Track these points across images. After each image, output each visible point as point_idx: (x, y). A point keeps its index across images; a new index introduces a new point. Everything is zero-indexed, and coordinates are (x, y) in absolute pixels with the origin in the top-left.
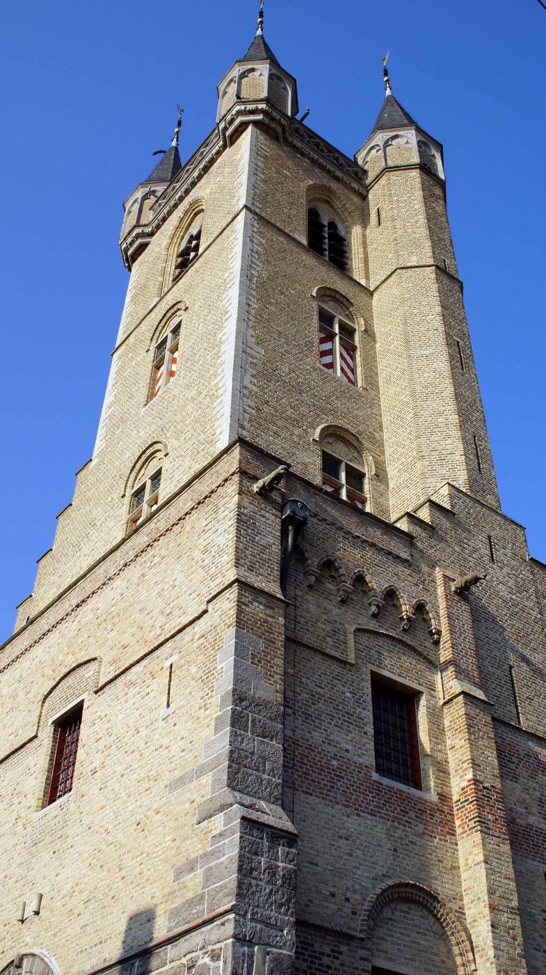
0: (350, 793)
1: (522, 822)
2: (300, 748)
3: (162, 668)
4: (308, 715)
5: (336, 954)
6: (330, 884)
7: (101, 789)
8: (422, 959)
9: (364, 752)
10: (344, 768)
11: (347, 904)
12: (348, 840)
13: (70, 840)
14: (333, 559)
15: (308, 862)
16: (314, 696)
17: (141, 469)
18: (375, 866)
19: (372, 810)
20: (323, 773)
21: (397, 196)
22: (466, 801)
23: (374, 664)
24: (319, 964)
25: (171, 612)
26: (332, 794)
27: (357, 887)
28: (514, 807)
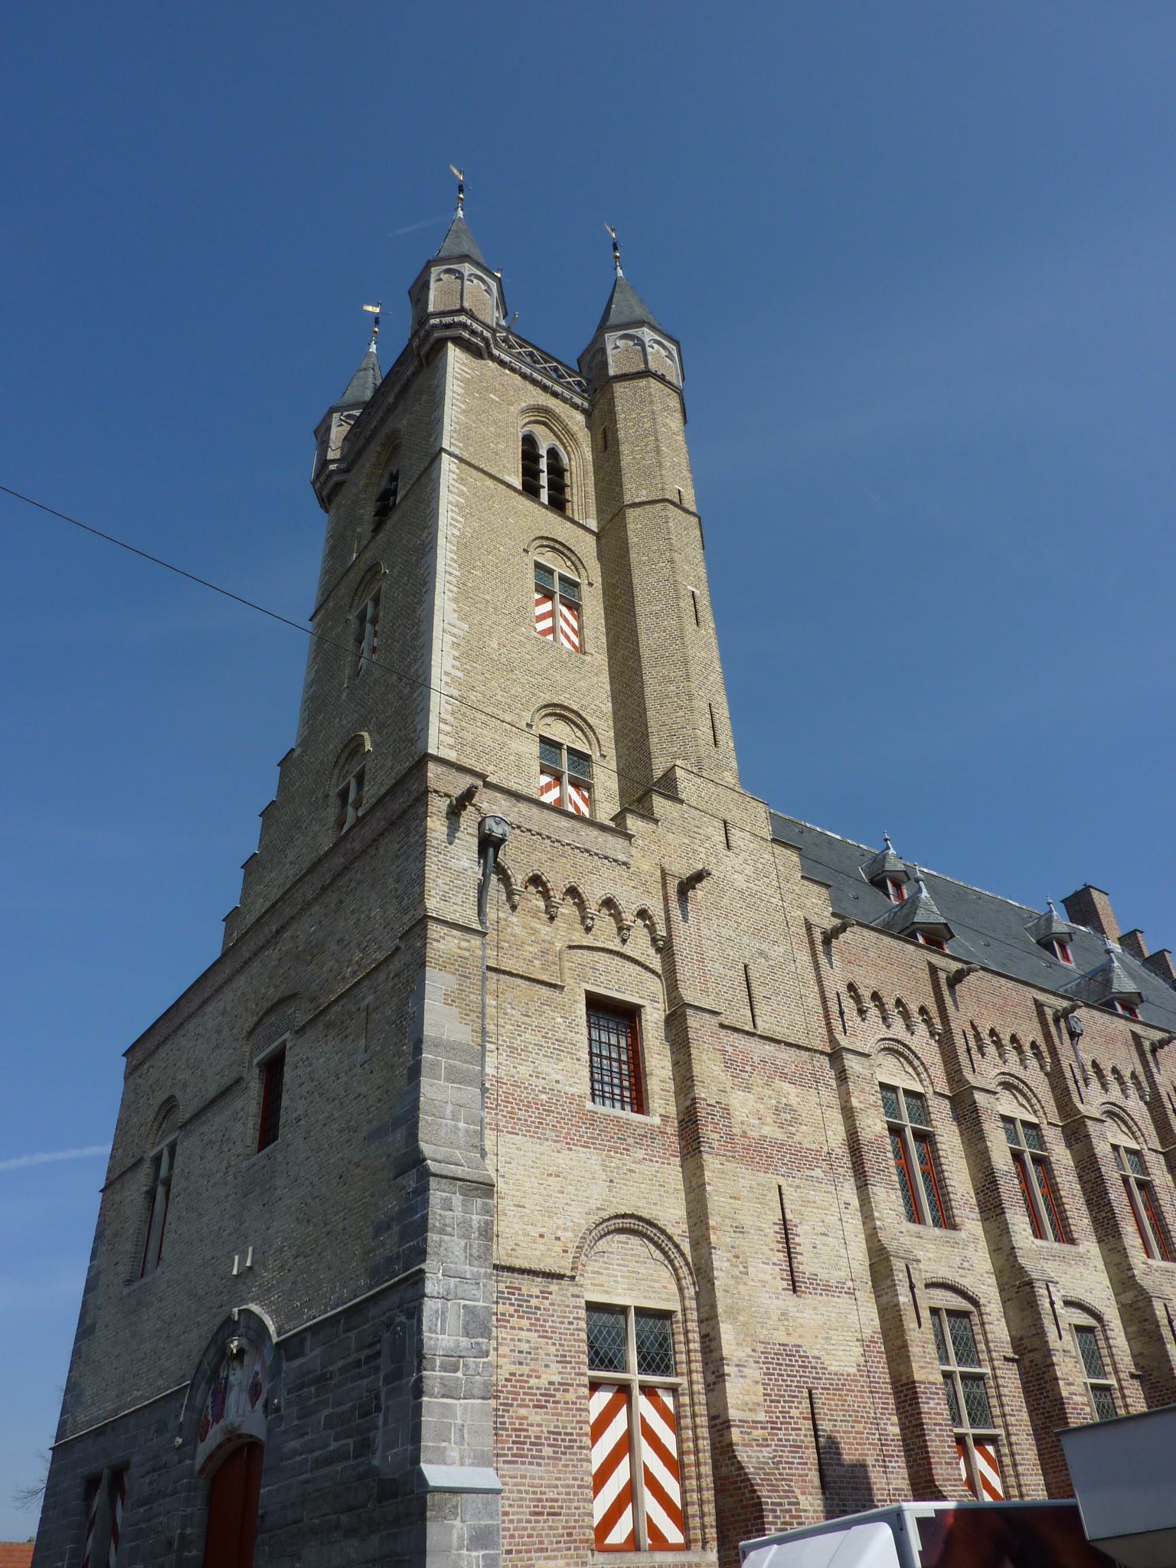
0: (561, 1127)
1: (754, 1134)
2: (504, 1086)
3: (359, 1009)
4: (514, 1048)
5: (545, 1294)
6: (539, 1225)
7: (305, 1138)
8: (641, 1287)
9: (578, 1081)
10: (554, 1101)
11: (558, 1242)
12: (559, 1176)
13: (278, 1192)
14: (539, 873)
15: (515, 1205)
16: (520, 1026)
17: (344, 764)
18: (589, 1200)
19: (585, 1142)
20: (530, 1110)
21: (624, 412)
22: (690, 1120)
23: (588, 982)
24: (527, 1307)
25: (367, 946)
26: (540, 1131)
27: (569, 1224)
28: (747, 1119)
